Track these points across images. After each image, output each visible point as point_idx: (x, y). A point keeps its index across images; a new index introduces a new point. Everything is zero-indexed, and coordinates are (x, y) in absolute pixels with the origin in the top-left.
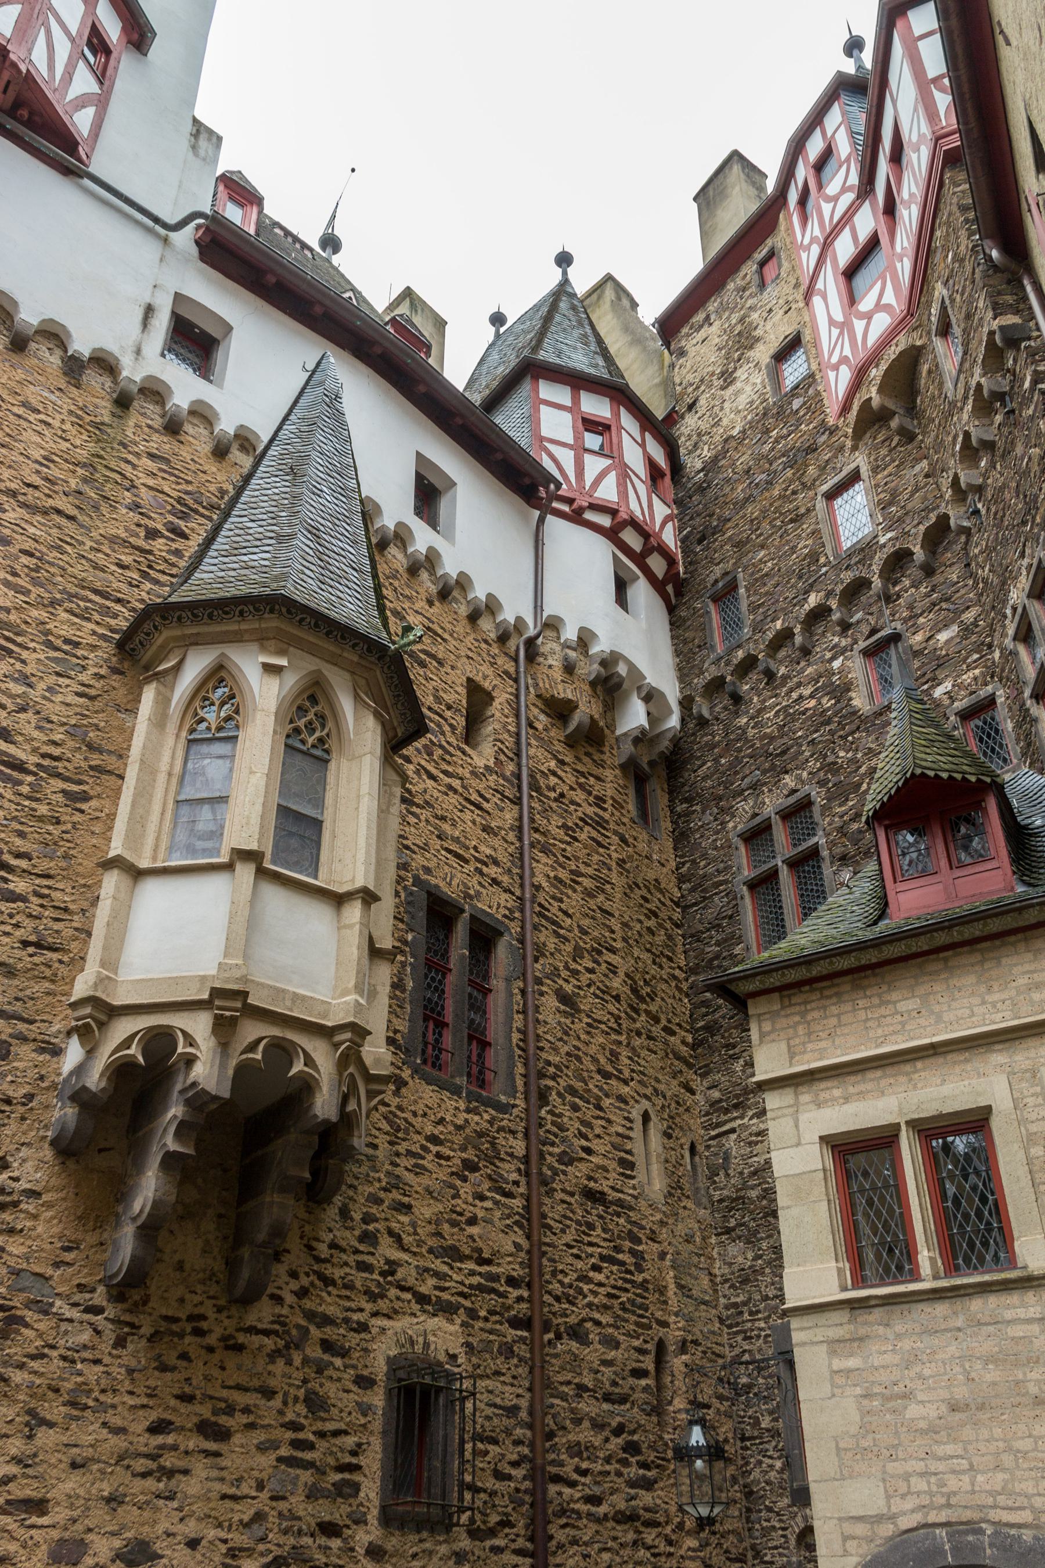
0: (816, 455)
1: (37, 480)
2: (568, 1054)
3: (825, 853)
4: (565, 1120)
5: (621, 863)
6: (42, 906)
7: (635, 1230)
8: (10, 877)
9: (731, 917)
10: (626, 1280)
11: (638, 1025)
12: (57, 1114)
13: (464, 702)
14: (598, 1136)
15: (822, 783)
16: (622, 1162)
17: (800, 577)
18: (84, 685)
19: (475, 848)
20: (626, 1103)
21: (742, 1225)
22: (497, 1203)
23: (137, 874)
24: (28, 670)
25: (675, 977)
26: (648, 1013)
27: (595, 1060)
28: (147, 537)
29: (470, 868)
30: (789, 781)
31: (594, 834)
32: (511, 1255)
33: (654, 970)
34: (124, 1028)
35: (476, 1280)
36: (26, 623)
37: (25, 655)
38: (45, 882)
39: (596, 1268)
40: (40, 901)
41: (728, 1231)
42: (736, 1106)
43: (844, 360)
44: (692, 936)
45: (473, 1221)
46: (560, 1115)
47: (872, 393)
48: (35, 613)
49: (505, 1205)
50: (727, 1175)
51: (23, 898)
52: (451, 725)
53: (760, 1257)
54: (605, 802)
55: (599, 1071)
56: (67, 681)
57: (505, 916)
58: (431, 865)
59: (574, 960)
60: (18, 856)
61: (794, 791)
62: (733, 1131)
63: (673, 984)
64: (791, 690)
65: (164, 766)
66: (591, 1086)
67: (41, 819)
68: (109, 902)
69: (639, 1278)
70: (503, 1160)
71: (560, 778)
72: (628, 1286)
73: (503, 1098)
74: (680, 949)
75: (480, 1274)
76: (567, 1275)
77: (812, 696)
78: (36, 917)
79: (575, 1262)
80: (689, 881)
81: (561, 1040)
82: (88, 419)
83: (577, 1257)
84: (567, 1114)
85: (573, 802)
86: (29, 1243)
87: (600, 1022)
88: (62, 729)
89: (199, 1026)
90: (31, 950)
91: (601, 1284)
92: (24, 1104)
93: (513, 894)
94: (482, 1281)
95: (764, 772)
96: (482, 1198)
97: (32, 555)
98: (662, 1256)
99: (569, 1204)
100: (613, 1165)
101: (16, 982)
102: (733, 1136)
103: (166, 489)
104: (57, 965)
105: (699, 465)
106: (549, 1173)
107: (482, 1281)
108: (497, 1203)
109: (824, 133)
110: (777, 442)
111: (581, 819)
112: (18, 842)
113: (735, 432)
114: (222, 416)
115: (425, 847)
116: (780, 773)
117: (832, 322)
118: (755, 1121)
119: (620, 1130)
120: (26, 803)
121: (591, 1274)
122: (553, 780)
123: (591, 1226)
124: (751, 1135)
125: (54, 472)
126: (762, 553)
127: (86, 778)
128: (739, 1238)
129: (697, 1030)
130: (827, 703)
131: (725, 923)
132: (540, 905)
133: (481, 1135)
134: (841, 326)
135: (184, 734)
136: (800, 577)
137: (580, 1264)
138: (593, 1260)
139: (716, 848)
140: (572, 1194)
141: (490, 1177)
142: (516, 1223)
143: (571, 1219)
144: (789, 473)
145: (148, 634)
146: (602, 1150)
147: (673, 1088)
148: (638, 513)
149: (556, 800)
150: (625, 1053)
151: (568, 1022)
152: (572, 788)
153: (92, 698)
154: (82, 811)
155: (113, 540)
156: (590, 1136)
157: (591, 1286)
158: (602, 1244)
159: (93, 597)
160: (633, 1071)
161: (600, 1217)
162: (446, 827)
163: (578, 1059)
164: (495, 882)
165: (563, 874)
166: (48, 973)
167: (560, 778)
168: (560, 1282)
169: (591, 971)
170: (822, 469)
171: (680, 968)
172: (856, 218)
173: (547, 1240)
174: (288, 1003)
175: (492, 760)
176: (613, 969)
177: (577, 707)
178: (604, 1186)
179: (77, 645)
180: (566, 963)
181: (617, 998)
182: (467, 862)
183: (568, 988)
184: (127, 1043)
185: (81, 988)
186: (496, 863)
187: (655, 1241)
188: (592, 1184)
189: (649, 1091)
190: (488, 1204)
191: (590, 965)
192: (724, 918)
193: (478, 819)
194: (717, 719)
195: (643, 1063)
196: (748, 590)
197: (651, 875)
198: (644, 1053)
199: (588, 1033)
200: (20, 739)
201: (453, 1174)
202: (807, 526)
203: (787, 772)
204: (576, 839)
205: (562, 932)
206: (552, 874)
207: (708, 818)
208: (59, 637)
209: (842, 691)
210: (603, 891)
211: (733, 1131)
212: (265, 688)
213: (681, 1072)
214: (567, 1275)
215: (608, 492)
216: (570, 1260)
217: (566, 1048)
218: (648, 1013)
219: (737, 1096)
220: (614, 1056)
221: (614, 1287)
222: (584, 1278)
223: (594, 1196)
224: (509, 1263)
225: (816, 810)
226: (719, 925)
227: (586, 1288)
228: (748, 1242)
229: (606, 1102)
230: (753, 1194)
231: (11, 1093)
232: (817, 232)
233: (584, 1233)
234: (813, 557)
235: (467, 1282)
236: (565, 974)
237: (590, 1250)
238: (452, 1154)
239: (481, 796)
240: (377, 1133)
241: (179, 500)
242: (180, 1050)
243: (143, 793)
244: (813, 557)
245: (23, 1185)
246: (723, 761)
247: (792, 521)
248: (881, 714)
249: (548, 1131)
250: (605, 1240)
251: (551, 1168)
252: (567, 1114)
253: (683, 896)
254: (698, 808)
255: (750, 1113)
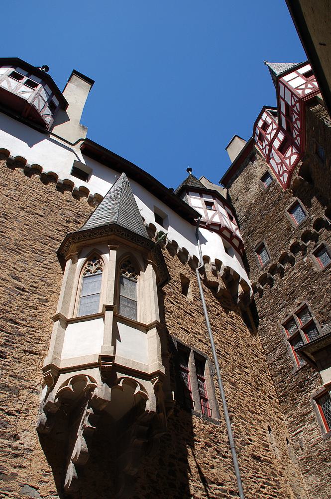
0: (282, 201)
1: (30, 205)
2: (237, 403)
3: (316, 322)
4: (241, 428)
5: (243, 338)
6: (31, 338)
7: (274, 471)
8: (19, 327)
9: (285, 353)
10: (274, 492)
11: (259, 394)
12: (38, 417)
13: (180, 280)
14: (253, 435)
15: (309, 299)
16: (264, 445)
17: (286, 236)
18: (45, 265)
19: (191, 328)
20: (261, 422)
21: (313, 468)
22: (221, 460)
23: (67, 323)
24: (26, 259)
25: (268, 379)
26: (262, 390)
27: (247, 407)
28: (66, 223)
29: (191, 335)
30: (297, 301)
31: (232, 327)
32: (229, 481)
33: (260, 375)
34: (63, 378)
35: (218, 492)
36: (26, 245)
37: (25, 254)
38: (32, 329)
39: (263, 487)
40: (30, 336)
41: (307, 471)
42: (301, 422)
43: (284, 172)
44: (271, 364)
45: (213, 467)
46: (238, 426)
47: (297, 176)
48: (29, 242)
49: (224, 461)
50: (302, 449)
51: (24, 335)
52: (177, 287)
53: (323, 479)
54: (233, 317)
55: (249, 410)
56: (40, 263)
57: (206, 352)
58: (176, 332)
59: (233, 370)
60: (22, 320)
61: (299, 304)
62: (302, 431)
63: (268, 381)
64: (291, 272)
65: (75, 285)
66: (247, 416)
67: (30, 307)
68: (56, 331)
69: (279, 491)
70: (220, 443)
71: (217, 308)
72: (276, 494)
73: (216, 419)
74: (268, 369)
75: (219, 489)
76: (252, 490)
77: (299, 272)
78: (28, 342)
79: (254, 484)
80: (266, 345)
81: (233, 398)
82: (47, 190)
83: (255, 482)
84: (241, 426)
85: (222, 316)
86: (28, 472)
87: (246, 392)
88: (38, 278)
89: (96, 373)
90: (27, 354)
91: (266, 494)
92: (25, 413)
93: (207, 345)
94: (220, 492)
95: (287, 301)
96: (215, 458)
97: (28, 225)
98: (286, 482)
99: (248, 461)
100: (261, 446)
101: (21, 365)
102: (302, 433)
103: (73, 210)
104: (37, 359)
105: (243, 214)
106: (238, 448)
107: (220, 492)
108: (221, 460)
109: (263, 120)
110: (268, 200)
111: (226, 322)
112: (22, 315)
113: (253, 202)
114: (90, 191)
115: (173, 326)
116: (293, 299)
117: (277, 164)
118: (310, 425)
119: (261, 433)
120: (25, 301)
121: (261, 489)
122: (214, 309)
123: (257, 470)
124: (309, 431)
125: (35, 203)
126: (270, 233)
127: (47, 295)
128: (313, 473)
129: (279, 397)
130: (305, 272)
131: (283, 356)
132: (217, 350)
133: (211, 433)
134: (281, 163)
135: (82, 275)
136: (286, 236)
137: (256, 485)
138: (261, 484)
139: (274, 331)
140: (249, 457)
141: (216, 450)
142: (229, 468)
143: (249, 467)
144: (274, 208)
145: (68, 247)
146: (256, 440)
147: (275, 418)
148: (227, 226)
149: (216, 315)
150: (257, 404)
151: (235, 392)
152: (221, 312)
153: (49, 269)
154: (46, 306)
155: (55, 223)
156: (251, 435)
157: (262, 495)
158: (263, 477)
159: (49, 238)
160: (261, 410)
161: (261, 466)
162: (180, 320)
163: (241, 405)
164: (200, 340)
165: (224, 340)
166: (34, 362)
167: (217, 308)
168: (250, 492)
169: (240, 374)
170: (285, 204)
171: (269, 376)
172: (278, 136)
173: (242, 475)
174: (131, 365)
175: (193, 300)
176: (247, 374)
177: (219, 284)
178: (259, 454)
179: (43, 252)
180: (230, 371)
181: (250, 384)
182: (189, 333)
183: (233, 380)
184: (66, 383)
185: (46, 362)
186: (199, 334)
187: (282, 476)
188: (255, 453)
189: (268, 418)
190: (217, 460)
191: (239, 372)
192: (283, 354)
193: (191, 319)
194: (266, 289)
195: (264, 408)
196: (268, 245)
197: (253, 343)
198: (263, 405)
199: (243, 396)
200: (23, 280)
201: (202, 448)
202: (284, 221)
203: (295, 299)
204: (226, 329)
205: (227, 360)
206: (220, 340)
207: (269, 321)
208: (37, 250)
209: (310, 267)
210: (238, 347)
211: (302, 431)
212: (110, 258)
213: (277, 412)
214: (252, 490)
215: (217, 219)
216: (252, 484)
217: (236, 401)
218: (262, 390)
219: (300, 418)
220: (254, 406)
221: (271, 495)
222: (258, 491)
223: (257, 458)
224: (230, 485)
225: (310, 308)
226: (281, 358)
227: (260, 495)
228: (317, 474)
229: (254, 422)
230: (315, 454)
231: (20, 408)
232: (267, 143)
233: (255, 472)
234: (289, 229)
235: (214, 493)
236: (231, 374)
237: (259, 479)
238: (200, 440)
239: (191, 311)
240: (8, 278)
241: (77, 213)
242: (88, 384)
243: (67, 294)
244: (289, 229)
245: (25, 446)
246: (271, 301)
247: (278, 221)
248: (325, 271)
249: (235, 432)
250: (264, 475)
251: (239, 447)
252: (241, 426)
253: (265, 351)
254: (265, 319)
255: (307, 423)
